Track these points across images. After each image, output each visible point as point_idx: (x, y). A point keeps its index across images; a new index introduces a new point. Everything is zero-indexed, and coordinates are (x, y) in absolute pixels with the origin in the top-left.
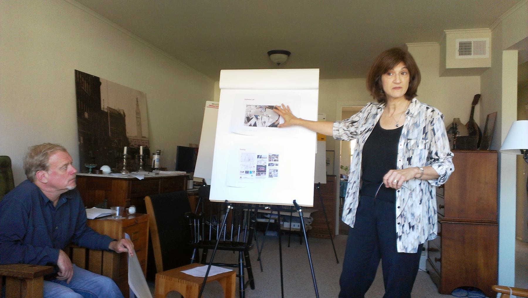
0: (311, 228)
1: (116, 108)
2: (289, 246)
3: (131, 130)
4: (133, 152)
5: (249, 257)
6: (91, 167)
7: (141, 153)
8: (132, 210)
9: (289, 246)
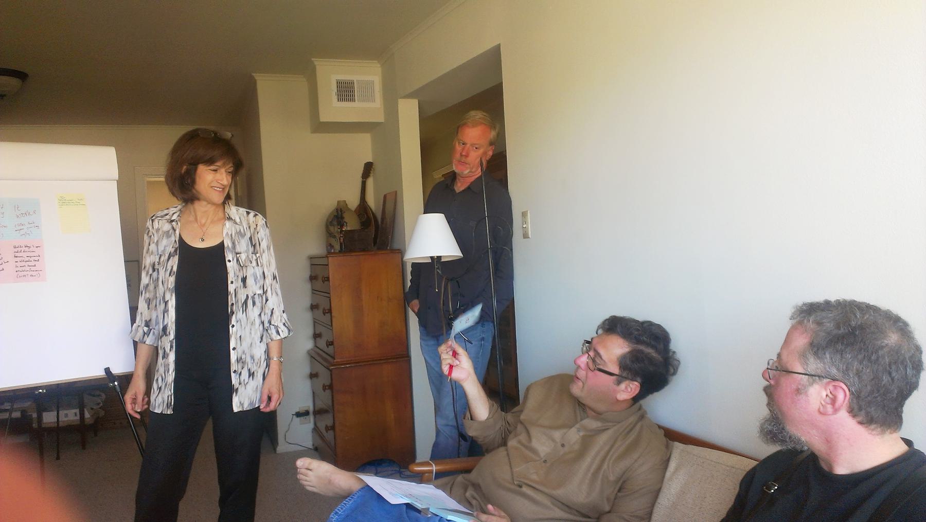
2: (58, 458)
9: (58, 458)
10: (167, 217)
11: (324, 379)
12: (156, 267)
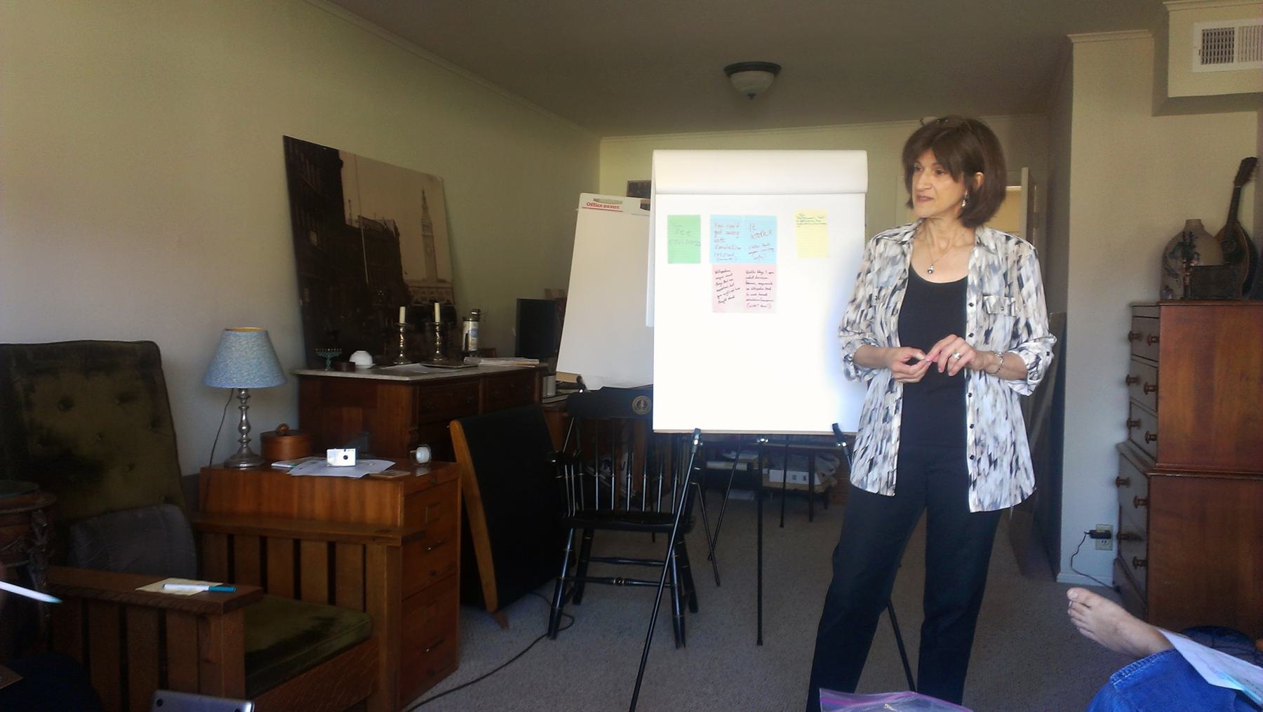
0: (834, 483)
1: (378, 218)
2: (782, 526)
3: (414, 268)
4: (420, 316)
5: (689, 569)
6: (330, 354)
7: (438, 319)
8: (423, 455)
9: (782, 526)
10: (897, 237)
11: (1139, 488)
12: (874, 303)
